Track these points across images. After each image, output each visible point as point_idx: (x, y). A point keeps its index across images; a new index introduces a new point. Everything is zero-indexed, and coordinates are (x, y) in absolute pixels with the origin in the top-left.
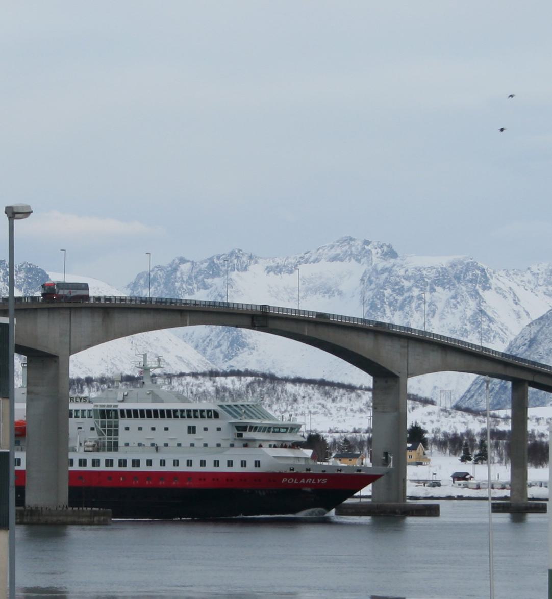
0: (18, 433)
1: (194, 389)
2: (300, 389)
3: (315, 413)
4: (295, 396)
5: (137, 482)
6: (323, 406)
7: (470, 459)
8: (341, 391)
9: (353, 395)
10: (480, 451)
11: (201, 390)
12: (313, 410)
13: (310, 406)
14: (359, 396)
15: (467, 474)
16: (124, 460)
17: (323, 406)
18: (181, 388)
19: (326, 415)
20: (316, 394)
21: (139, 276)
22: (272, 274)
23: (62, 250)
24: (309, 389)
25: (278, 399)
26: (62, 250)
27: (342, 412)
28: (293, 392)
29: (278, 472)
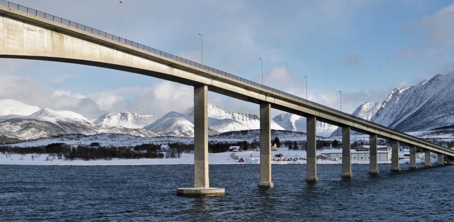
0: (193, 185)
1: (256, 133)
2: (279, 132)
3: (282, 138)
4: (278, 134)
5: (117, 150)
6: (284, 136)
7: (292, 149)
8: (289, 133)
9: (291, 133)
10: (338, 144)
11: (257, 133)
12: (281, 137)
13: (281, 136)
14: (292, 134)
15: (281, 154)
16: (194, 186)
17: (284, 136)
18: (253, 133)
19: (284, 138)
20: (283, 133)
21: (276, 117)
22: (210, 137)
23: (339, 91)
24: (281, 132)
25: (274, 135)
26: (339, 91)
27: (288, 137)
28: (277, 133)
29: (113, 159)
